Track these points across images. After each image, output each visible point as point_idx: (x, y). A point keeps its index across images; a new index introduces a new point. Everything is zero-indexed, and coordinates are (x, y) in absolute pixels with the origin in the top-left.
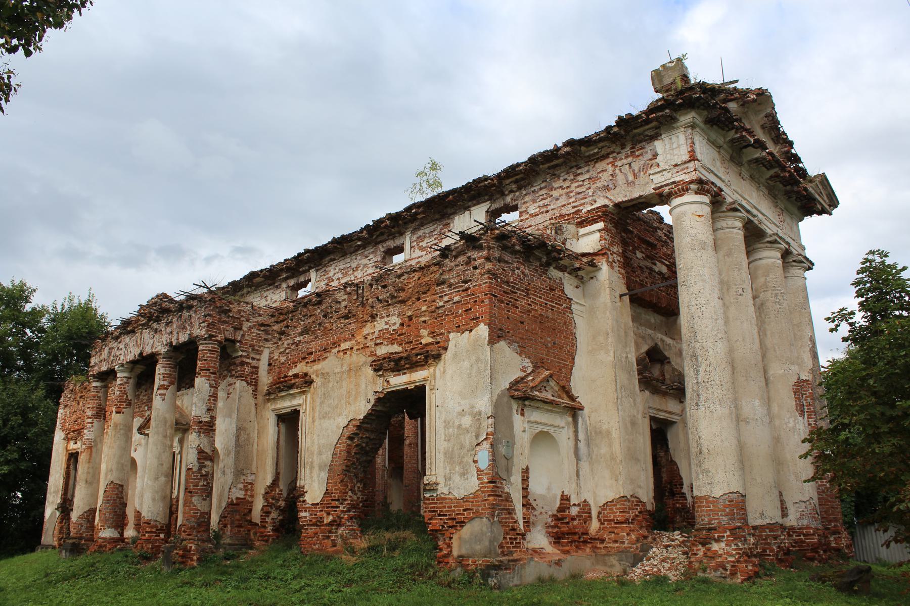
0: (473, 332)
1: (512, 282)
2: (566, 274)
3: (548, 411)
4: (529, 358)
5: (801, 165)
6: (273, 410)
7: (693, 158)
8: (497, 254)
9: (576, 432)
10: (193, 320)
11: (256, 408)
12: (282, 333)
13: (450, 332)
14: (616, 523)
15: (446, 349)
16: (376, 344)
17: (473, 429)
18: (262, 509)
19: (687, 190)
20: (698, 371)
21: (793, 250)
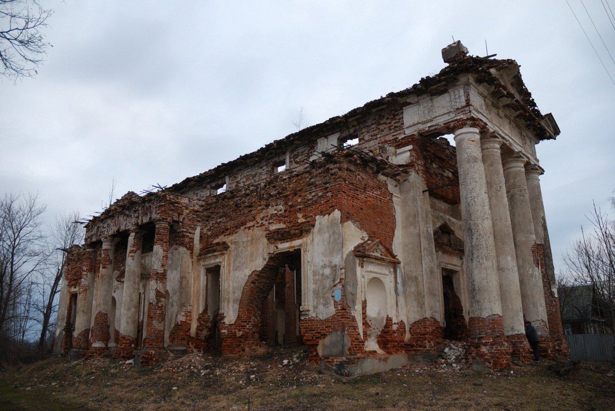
0: (331, 215)
2: (389, 178)
3: (378, 264)
4: (366, 231)
5: (536, 108)
6: (203, 266)
9: (396, 278)
10: (152, 209)
11: (193, 264)
13: (316, 215)
15: (313, 226)
16: (269, 223)
18: (197, 328)
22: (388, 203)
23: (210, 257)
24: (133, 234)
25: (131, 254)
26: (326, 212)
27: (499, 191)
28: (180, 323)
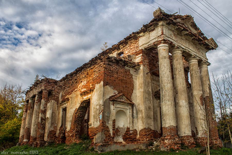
1: (112, 70)
2: (131, 68)
3: (122, 104)
4: (117, 90)
6: (62, 108)
7: (163, 34)
8: (107, 63)
9: (133, 111)
12: (64, 88)
13: (95, 84)
14: (143, 136)
15: (95, 88)
16: (81, 89)
17: (99, 109)
19: (161, 43)
20: (163, 92)
21: (203, 60)
22: (130, 79)
23: (63, 104)
24: (37, 96)
25: (36, 104)
26: (98, 83)
27: (180, 71)
28: (51, 131)
